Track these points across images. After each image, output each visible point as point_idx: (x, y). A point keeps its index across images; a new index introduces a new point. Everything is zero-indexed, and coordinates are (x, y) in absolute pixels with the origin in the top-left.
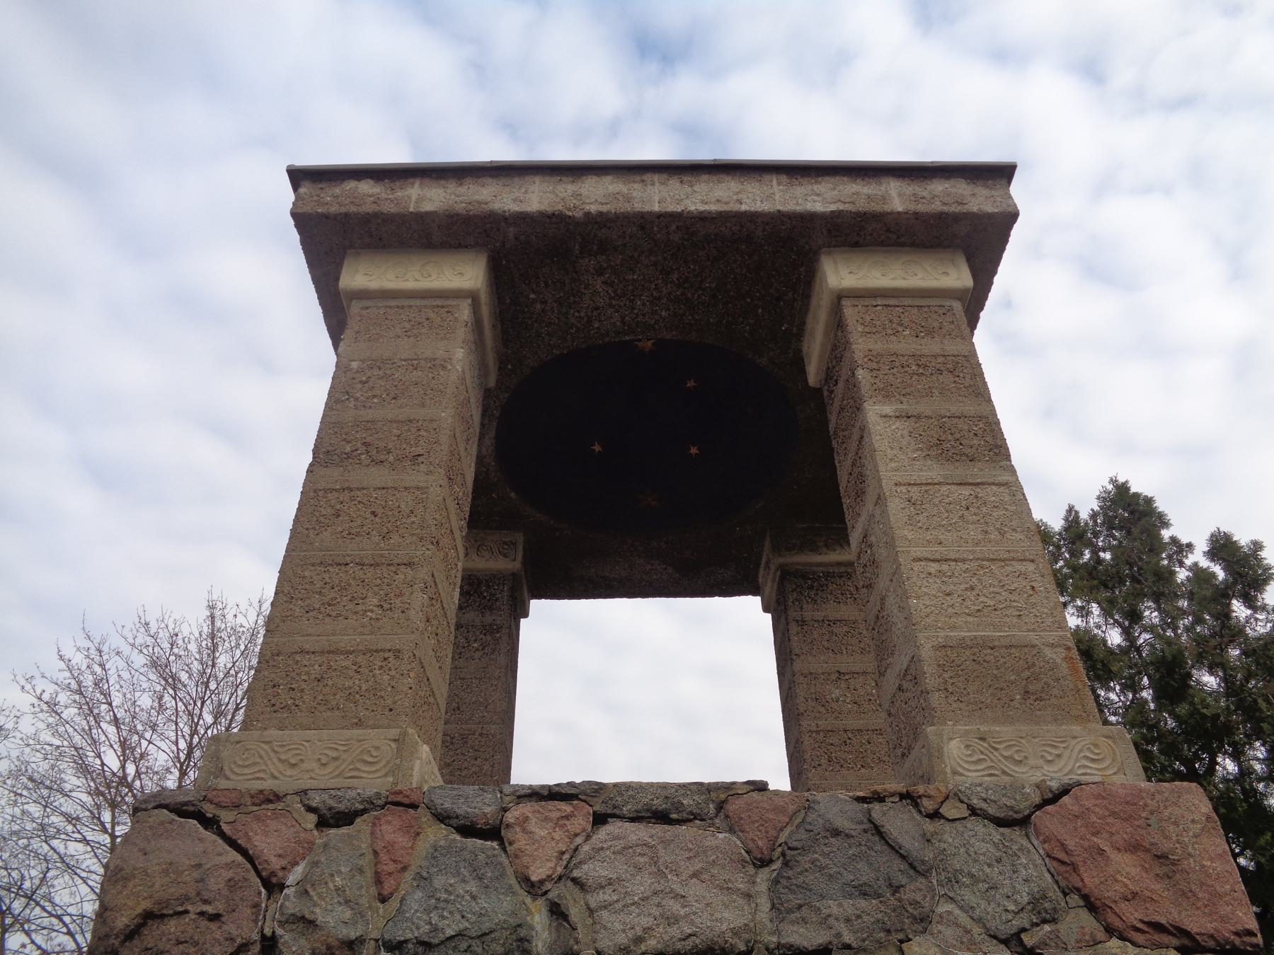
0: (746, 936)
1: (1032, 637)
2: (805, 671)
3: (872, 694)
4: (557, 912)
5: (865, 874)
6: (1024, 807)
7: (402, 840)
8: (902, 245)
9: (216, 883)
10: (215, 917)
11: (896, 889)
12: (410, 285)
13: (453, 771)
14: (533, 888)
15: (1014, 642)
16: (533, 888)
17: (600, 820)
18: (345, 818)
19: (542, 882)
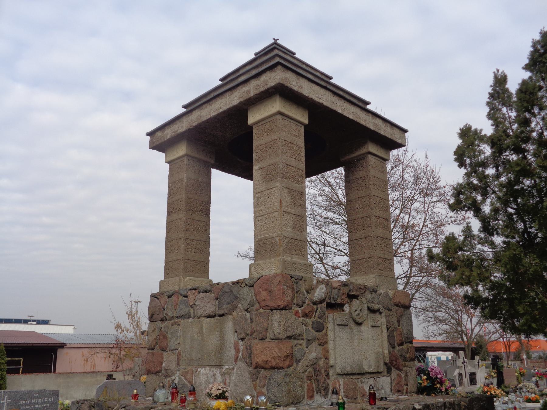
0: (214, 312)
1: (274, 235)
2: (349, 200)
3: (367, 204)
8: (265, 99)
10: (158, 314)
11: (233, 302)
15: (271, 237)
19: (192, 305)
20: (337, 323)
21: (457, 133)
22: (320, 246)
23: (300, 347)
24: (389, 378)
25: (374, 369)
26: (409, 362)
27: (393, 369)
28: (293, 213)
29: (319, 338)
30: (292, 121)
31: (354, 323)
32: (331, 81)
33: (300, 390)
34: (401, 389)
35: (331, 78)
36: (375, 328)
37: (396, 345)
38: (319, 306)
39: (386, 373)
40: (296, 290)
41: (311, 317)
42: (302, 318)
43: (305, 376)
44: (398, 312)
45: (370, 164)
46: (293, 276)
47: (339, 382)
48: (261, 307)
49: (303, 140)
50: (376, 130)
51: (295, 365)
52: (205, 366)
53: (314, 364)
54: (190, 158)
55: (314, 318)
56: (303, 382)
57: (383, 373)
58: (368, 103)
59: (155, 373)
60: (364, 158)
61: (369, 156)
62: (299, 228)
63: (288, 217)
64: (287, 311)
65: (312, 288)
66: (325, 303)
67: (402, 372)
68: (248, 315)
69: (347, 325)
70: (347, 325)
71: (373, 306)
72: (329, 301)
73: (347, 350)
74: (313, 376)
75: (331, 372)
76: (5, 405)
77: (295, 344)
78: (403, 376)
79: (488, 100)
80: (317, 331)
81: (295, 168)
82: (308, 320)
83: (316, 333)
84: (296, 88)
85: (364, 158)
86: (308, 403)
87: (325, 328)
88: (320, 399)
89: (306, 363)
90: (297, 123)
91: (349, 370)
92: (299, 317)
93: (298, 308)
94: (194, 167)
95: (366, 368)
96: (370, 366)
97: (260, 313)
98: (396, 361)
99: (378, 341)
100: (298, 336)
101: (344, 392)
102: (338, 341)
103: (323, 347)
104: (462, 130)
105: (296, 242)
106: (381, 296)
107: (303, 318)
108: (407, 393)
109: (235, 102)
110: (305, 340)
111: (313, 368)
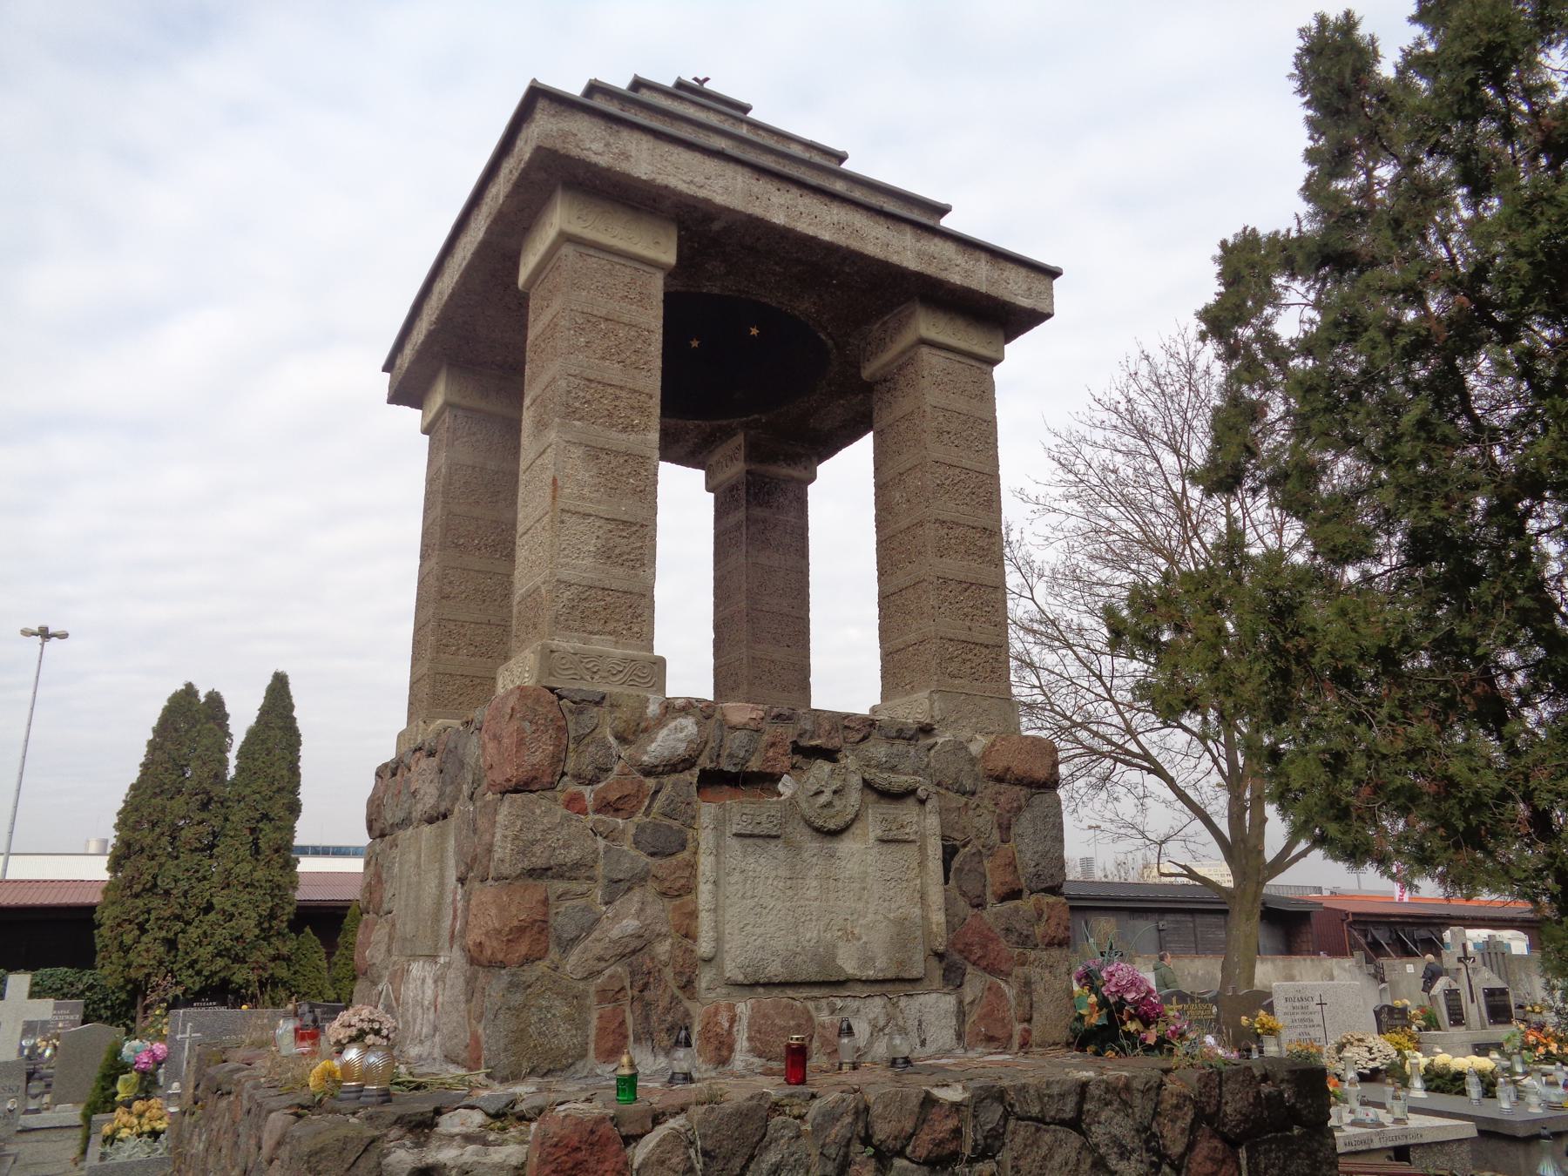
20: (734, 831)
21: (1214, 259)
23: (581, 902)
24: (948, 1002)
25: (881, 970)
26: (1042, 950)
27: (970, 968)
28: (602, 514)
29: (659, 875)
30: (616, 259)
31: (808, 831)
32: (846, 166)
33: (568, 1030)
34: (998, 1033)
35: (841, 158)
36: (893, 847)
37: (990, 898)
38: (668, 781)
39: (937, 980)
40: (572, 734)
41: (631, 815)
42: (592, 817)
43: (592, 989)
44: (1002, 799)
45: (925, 373)
46: (565, 693)
47: (731, 1007)
49: (659, 311)
50: (931, 270)
51: (554, 954)
53: (634, 950)
54: (460, 413)
55: (647, 813)
56: (581, 1009)
57: (926, 982)
58: (943, 210)
60: (912, 359)
61: (925, 350)
62: (625, 557)
63: (581, 528)
64: (534, 796)
65: (643, 725)
66: (696, 771)
67: (1006, 981)
69: (777, 837)
70: (777, 837)
71: (882, 779)
72: (709, 766)
73: (775, 912)
74: (623, 988)
75: (705, 978)
76: (187, 1046)
77: (559, 892)
78: (1010, 991)
79: (1310, 144)
80: (652, 855)
81: (621, 388)
82: (620, 821)
83: (649, 860)
84: (603, 161)
85: (911, 361)
86: (599, 1071)
87: (690, 846)
88: (651, 1059)
89: (598, 949)
90: (637, 265)
91: (775, 970)
92: (584, 811)
93: (582, 788)
94: (474, 434)
95: (849, 965)
96: (866, 961)
98: (984, 947)
99: (905, 885)
100: (571, 869)
101: (750, 1039)
102: (737, 883)
103: (677, 902)
105: (608, 599)
106: (932, 752)
107: (597, 817)
108: (1024, 1044)
109: (481, 235)
110: (602, 882)
111: (630, 965)
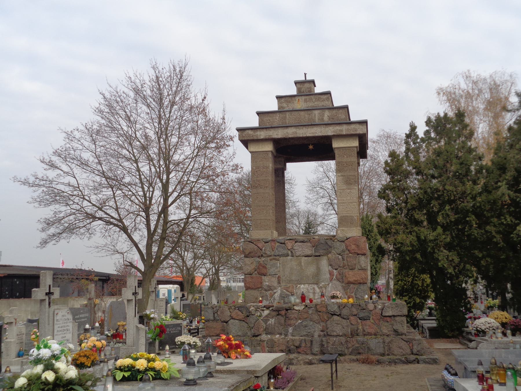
1: (353, 215)
4: (292, 252)
5: (325, 248)
6: (344, 240)
7: (274, 245)
9: (255, 250)
12: (260, 150)
13: (280, 234)
14: (289, 250)
16: (289, 250)
17: (296, 242)
18: (268, 242)
22: (94, 152)
48: (350, 253)
52: (304, 284)
59: (255, 289)
68: (340, 257)
97: (350, 256)
104: (426, 122)
